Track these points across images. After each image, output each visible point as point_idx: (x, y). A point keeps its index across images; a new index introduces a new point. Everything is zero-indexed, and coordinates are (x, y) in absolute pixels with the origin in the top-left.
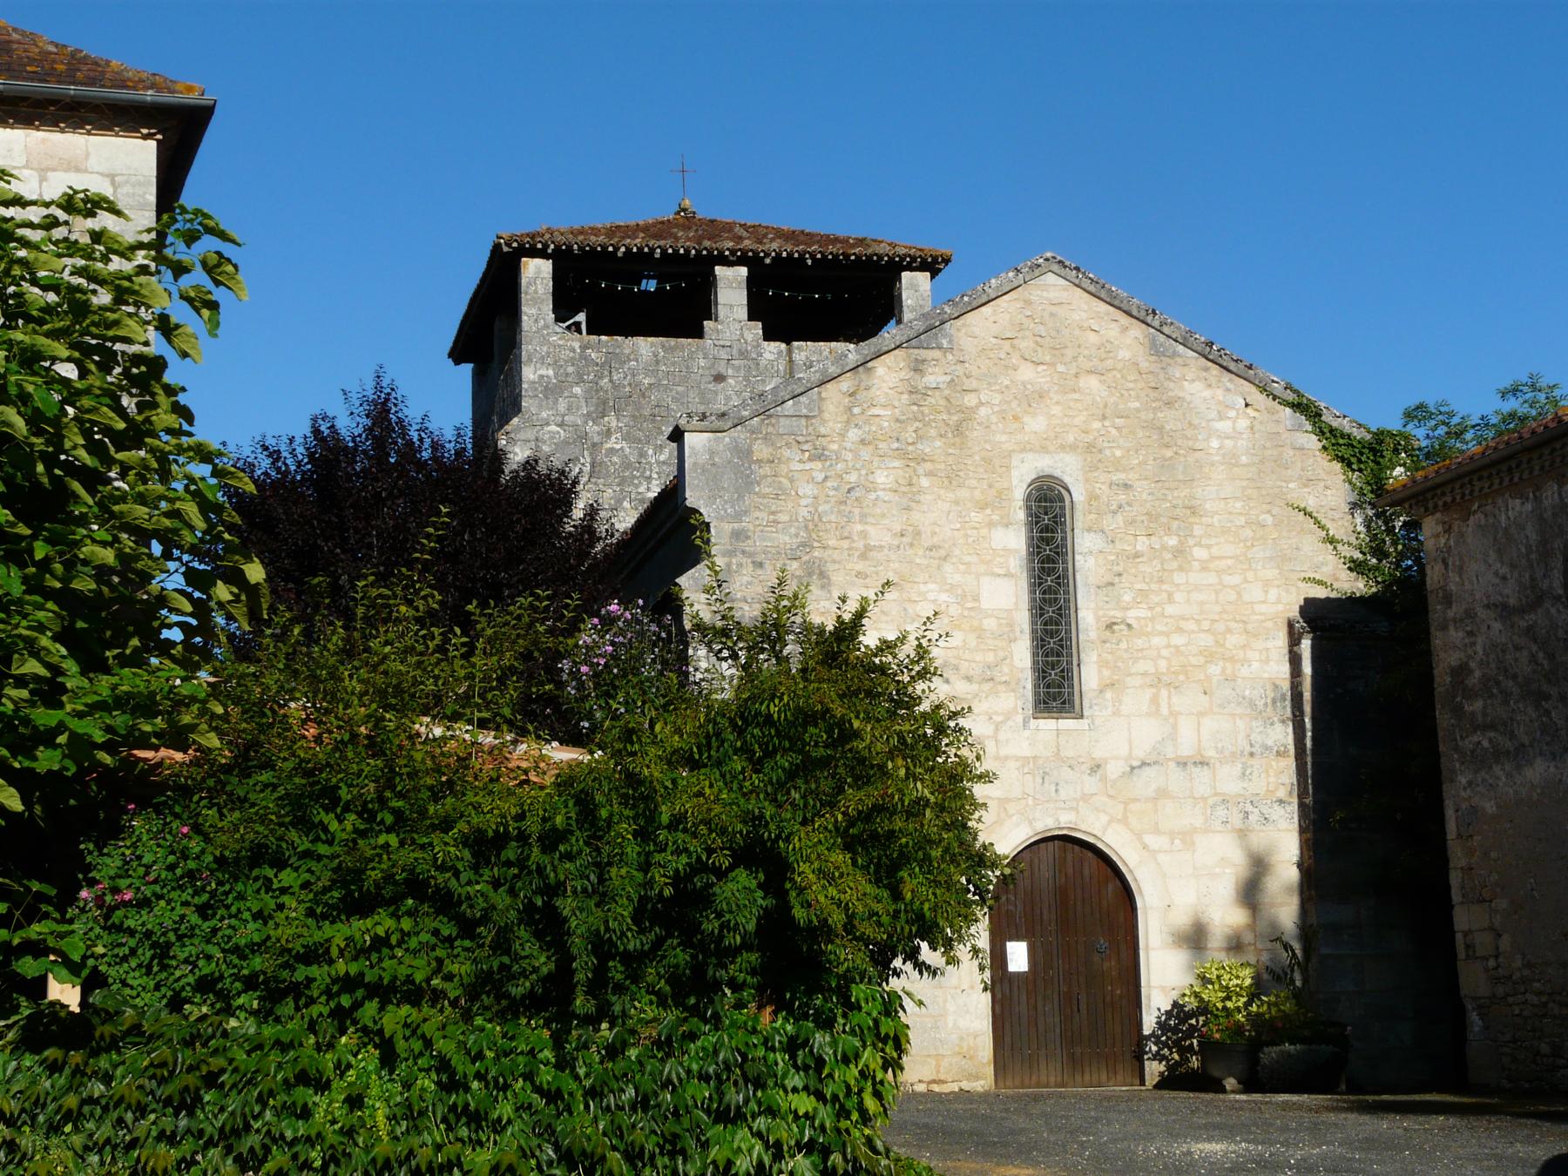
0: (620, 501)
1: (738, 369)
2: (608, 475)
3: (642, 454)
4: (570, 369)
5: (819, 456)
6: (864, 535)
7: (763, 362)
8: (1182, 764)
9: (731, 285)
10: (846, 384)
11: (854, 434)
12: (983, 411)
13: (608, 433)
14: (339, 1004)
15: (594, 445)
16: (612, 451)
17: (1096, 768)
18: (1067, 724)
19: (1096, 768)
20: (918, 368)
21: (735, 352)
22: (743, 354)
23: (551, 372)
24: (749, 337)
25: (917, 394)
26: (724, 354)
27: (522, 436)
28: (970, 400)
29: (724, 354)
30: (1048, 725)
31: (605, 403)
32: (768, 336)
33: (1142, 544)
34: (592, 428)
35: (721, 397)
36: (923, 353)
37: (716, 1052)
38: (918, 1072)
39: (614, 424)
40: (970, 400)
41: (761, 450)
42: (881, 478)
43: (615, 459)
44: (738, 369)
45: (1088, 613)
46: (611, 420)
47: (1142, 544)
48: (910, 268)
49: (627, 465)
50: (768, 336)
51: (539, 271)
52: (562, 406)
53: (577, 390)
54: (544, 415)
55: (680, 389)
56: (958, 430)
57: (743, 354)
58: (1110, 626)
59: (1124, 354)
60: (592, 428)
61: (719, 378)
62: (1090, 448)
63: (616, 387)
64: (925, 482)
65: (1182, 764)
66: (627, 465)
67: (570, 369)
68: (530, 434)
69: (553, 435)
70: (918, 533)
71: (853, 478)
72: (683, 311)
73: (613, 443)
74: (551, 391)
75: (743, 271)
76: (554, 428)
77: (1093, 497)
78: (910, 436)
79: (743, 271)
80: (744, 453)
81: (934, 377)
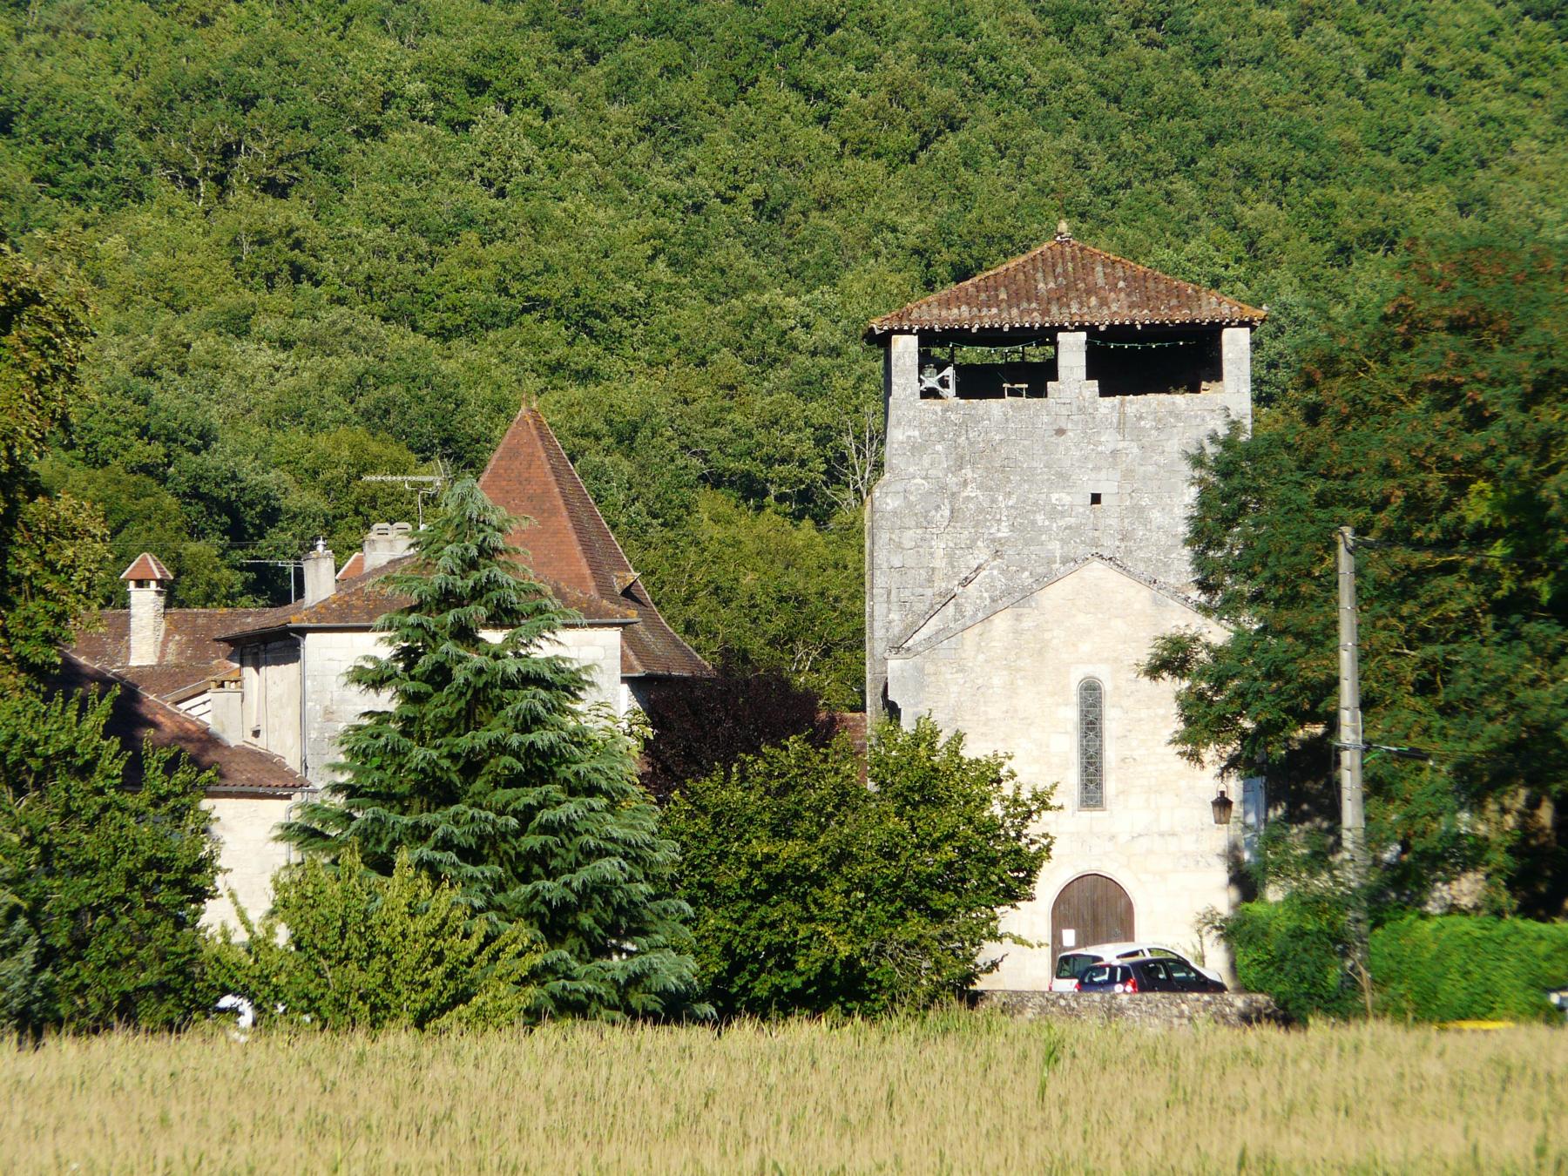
0: (974, 541)
1: (1077, 423)
2: (964, 520)
3: (993, 501)
4: (933, 430)
5: (961, 670)
6: (986, 713)
7: (1099, 416)
8: (1162, 835)
9: (1072, 351)
10: (977, 630)
11: (981, 657)
12: (1055, 641)
13: (965, 483)
14: (1082, 941)
15: (953, 494)
16: (968, 498)
17: (1112, 838)
18: (1096, 814)
19: (1112, 838)
20: (1018, 618)
21: (1074, 409)
22: (1081, 410)
23: (917, 433)
24: (1087, 394)
25: (1017, 633)
26: (1064, 411)
27: (892, 488)
28: (1047, 636)
29: (1064, 411)
30: (1087, 815)
31: (962, 458)
32: (1104, 392)
33: (1144, 714)
34: (952, 480)
35: (1062, 448)
36: (1020, 610)
37: (360, 933)
38: (215, 916)
39: (970, 475)
40: (1047, 636)
41: (930, 668)
42: (996, 681)
43: (971, 506)
44: (1077, 423)
45: (1111, 754)
46: (968, 472)
47: (1144, 714)
48: (1228, 325)
49: (981, 510)
50: (1104, 392)
51: (907, 347)
52: (926, 461)
53: (939, 448)
54: (911, 470)
55: (1026, 443)
56: (1040, 652)
57: (1081, 410)
58: (1123, 760)
59: (1137, 606)
60: (952, 480)
61: (1060, 432)
62: (1116, 660)
63: (971, 444)
64: (1020, 683)
65: (1162, 835)
66: (981, 510)
67: (933, 430)
68: (899, 487)
69: (918, 487)
70: (1016, 711)
71: (980, 681)
72: (1038, 378)
73: (970, 491)
74: (917, 449)
75: (1083, 336)
76: (918, 481)
77: (1117, 688)
78: (1012, 657)
79: (1083, 336)
80: (920, 670)
81: (1027, 623)
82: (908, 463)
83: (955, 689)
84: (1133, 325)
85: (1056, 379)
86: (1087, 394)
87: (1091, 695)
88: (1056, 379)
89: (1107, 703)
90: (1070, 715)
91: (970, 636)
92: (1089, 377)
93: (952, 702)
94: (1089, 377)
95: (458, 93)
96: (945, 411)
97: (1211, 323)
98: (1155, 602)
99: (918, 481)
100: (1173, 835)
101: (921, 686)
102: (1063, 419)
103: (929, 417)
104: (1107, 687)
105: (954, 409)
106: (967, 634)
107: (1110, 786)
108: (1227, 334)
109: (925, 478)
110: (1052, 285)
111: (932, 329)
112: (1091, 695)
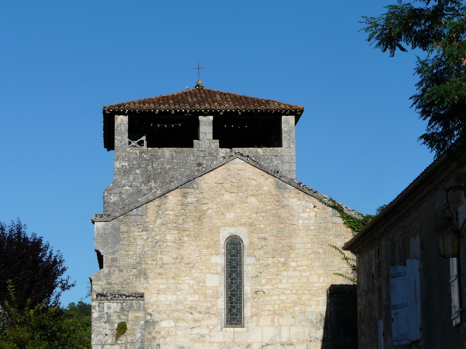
4: (135, 162)
5: (145, 230)
6: (162, 259)
8: (283, 344)
9: (206, 125)
10: (156, 202)
11: (159, 221)
12: (209, 211)
20: (185, 196)
21: (207, 153)
22: (210, 154)
23: (126, 164)
24: (213, 146)
27: (114, 191)
28: (205, 207)
31: (150, 176)
32: (222, 146)
33: (270, 261)
34: (144, 187)
36: (187, 190)
39: (153, 185)
40: (205, 207)
41: (123, 228)
42: (169, 237)
45: (248, 288)
46: (152, 184)
47: (270, 261)
51: (122, 121)
53: (138, 171)
54: (123, 182)
55: (182, 170)
56: (199, 219)
57: (210, 154)
58: (256, 292)
59: (266, 188)
62: (251, 224)
63: (154, 170)
64: (186, 239)
65: (283, 344)
67: (135, 162)
68: (117, 191)
70: (182, 258)
71: (158, 238)
76: (127, 188)
77: (251, 243)
78: (181, 221)
79: (211, 118)
82: (122, 179)
83: (140, 242)
84: (236, 112)
85: (198, 139)
86: (213, 146)
87: (234, 249)
88: (198, 139)
89: (246, 252)
90: (220, 261)
91: (152, 206)
92: (214, 138)
93: (139, 251)
94: (214, 138)
95: (85, 326)
96: (141, 153)
97: (276, 111)
98: (278, 186)
99: (127, 188)
100: (291, 344)
101: (117, 240)
102: (201, 158)
103: (133, 156)
104: (246, 242)
105: (146, 153)
106: (151, 205)
107: (247, 311)
108: (284, 118)
109: (130, 186)
110: (195, 100)
111: (135, 111)
112: (234, 249)
